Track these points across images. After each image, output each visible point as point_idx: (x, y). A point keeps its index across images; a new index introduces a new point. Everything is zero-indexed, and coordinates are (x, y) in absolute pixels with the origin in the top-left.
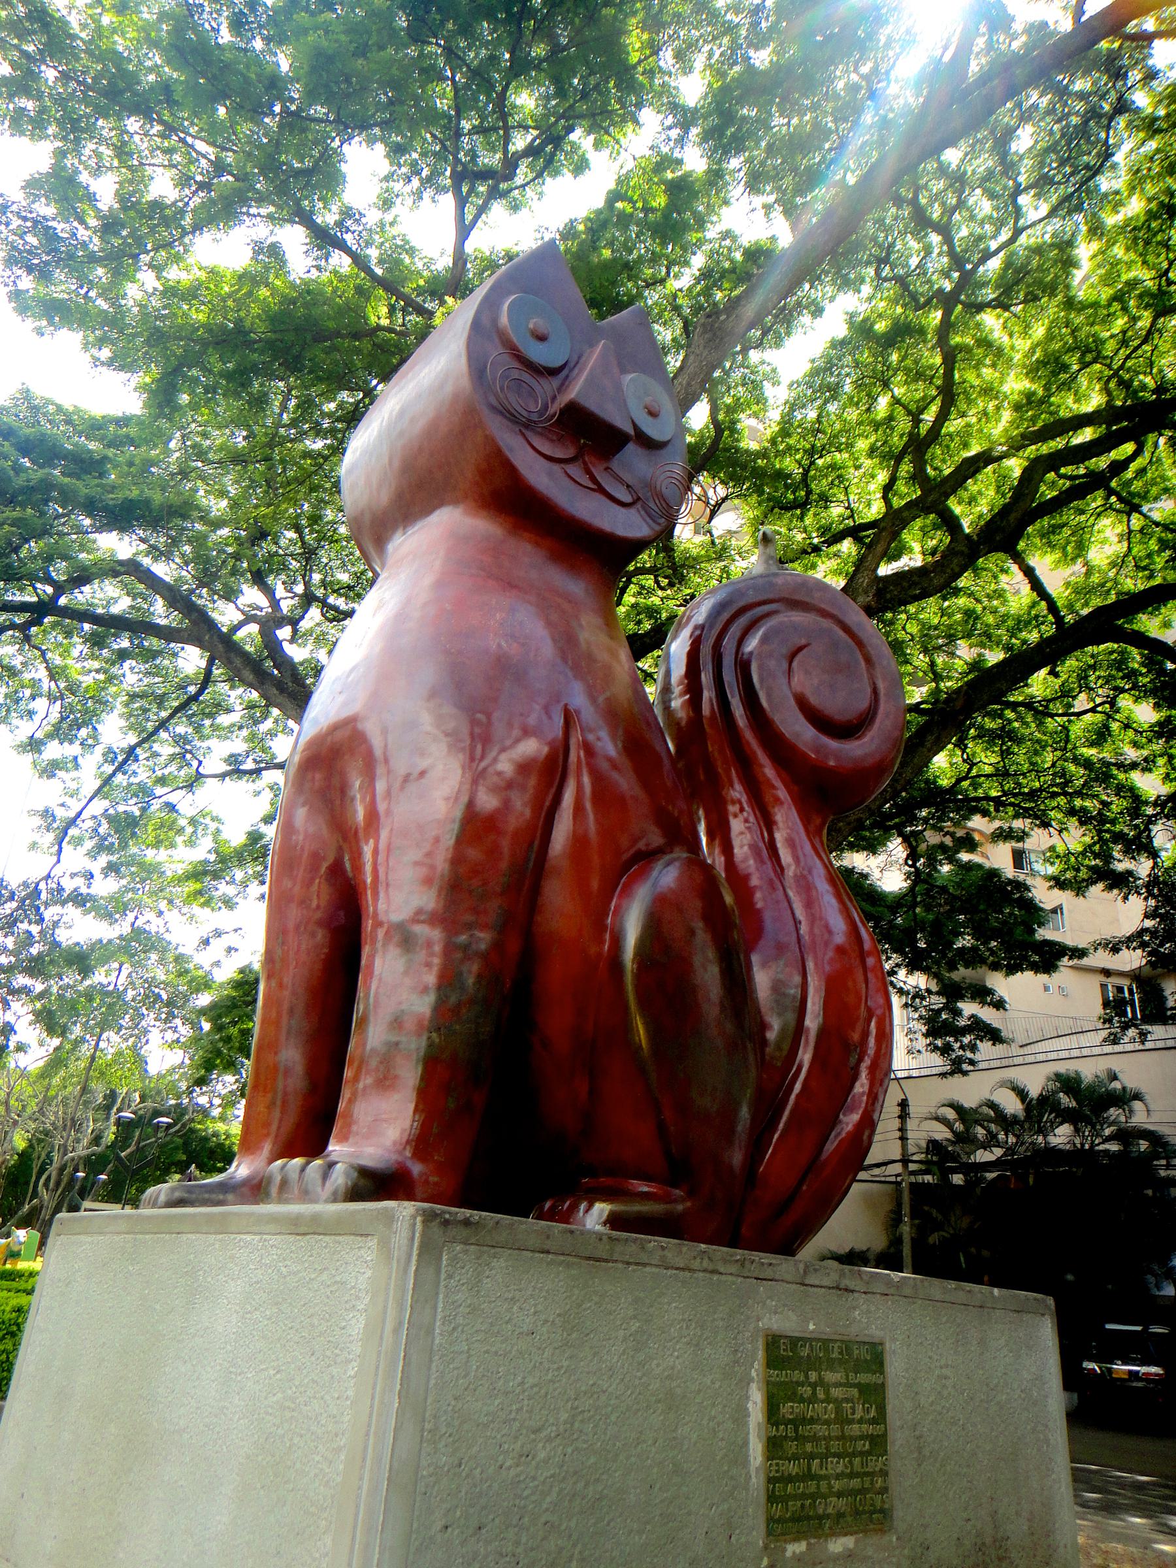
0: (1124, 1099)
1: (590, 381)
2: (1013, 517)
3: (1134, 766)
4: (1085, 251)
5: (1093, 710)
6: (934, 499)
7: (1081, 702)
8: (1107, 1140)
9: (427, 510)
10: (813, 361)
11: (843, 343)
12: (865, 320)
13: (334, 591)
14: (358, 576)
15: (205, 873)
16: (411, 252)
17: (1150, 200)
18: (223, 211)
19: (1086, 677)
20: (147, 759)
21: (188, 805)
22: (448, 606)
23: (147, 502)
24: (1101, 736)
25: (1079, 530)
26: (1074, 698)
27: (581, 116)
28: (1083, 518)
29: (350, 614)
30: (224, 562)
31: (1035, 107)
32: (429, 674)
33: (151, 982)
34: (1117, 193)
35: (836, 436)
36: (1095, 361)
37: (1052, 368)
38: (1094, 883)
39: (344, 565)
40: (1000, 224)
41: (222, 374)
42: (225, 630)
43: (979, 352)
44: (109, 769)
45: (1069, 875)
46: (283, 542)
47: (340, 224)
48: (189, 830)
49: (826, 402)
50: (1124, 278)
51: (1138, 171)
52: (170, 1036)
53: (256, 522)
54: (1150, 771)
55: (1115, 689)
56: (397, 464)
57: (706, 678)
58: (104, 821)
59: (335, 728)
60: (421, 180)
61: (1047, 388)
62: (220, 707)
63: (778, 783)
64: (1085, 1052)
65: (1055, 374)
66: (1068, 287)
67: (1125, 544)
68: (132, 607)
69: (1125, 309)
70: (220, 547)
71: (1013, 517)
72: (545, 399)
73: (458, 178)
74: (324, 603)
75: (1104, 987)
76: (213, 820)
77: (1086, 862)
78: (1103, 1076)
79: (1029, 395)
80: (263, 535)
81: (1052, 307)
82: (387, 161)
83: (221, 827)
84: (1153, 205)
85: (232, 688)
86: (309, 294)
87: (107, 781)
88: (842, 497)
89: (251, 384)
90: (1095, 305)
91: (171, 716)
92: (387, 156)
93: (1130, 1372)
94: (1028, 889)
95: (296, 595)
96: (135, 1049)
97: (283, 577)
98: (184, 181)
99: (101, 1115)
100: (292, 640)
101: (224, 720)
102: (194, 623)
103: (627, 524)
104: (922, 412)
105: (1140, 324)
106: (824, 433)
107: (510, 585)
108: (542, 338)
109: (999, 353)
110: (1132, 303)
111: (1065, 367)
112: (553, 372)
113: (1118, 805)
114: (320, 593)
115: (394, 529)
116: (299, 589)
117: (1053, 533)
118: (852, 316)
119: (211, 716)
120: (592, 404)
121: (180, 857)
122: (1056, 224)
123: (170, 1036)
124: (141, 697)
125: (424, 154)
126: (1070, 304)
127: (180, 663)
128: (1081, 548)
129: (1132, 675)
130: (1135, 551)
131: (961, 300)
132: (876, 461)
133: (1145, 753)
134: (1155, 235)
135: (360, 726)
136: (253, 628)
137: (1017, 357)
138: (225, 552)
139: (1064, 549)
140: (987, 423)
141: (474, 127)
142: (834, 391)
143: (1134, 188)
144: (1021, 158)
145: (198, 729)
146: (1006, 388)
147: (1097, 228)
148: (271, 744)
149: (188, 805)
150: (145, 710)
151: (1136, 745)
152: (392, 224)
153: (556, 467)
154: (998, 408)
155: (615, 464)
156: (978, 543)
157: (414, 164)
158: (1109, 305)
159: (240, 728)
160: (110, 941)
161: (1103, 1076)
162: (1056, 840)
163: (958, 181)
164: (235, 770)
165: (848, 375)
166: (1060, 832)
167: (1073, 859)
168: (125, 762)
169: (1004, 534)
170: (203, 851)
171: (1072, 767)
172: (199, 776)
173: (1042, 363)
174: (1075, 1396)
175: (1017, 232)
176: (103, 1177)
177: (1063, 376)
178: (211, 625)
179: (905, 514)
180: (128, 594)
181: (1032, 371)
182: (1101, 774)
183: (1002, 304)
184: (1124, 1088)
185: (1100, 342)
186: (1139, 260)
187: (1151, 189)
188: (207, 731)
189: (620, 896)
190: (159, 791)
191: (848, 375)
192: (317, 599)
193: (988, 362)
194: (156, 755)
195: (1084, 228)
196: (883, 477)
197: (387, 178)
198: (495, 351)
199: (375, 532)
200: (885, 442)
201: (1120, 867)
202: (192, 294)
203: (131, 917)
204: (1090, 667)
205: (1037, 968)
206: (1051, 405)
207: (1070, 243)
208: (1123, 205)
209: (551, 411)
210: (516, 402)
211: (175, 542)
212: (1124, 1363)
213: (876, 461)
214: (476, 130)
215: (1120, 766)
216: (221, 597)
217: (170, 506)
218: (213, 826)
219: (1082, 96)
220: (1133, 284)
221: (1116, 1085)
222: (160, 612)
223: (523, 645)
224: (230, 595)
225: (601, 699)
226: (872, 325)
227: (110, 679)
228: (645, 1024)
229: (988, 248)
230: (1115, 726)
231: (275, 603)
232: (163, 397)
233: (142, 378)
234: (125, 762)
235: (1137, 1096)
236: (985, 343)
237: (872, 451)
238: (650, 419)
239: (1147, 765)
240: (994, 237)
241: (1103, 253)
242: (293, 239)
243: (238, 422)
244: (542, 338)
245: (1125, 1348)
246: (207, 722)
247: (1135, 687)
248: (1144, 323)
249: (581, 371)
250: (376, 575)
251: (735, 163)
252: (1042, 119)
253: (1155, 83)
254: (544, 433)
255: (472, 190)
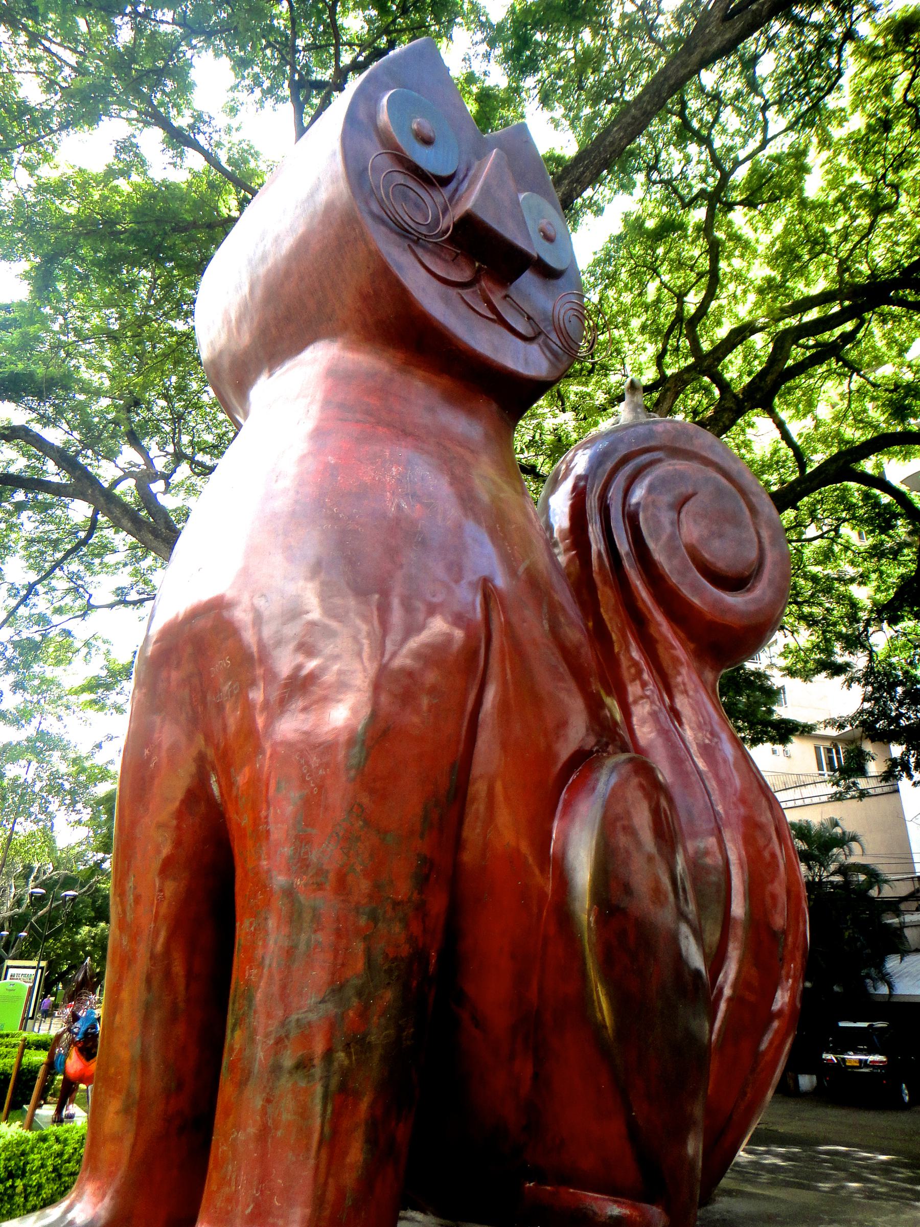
0: (843, 841)
1: (486, 191)
2: (769, 379)
3: (852, 580)
4: (815, 158)
5: (821, 537)
6: (708, 364)
7: (811, 531)
8: (833, 874)
9: (296, 346)
10: (595, 253)
11: (619, 238)
12: (638, 218)
13: (200, 450)
14: (220, 437)
15: (98, 686)
16: (256, 155)
17: (871, 116)
18: (86, 106)
19: (815, 510)
20: (46, 593)
21: (81, 630)
22: (331, 460)
23: (31, 375)
24: (827, 556)
25: (810, 390)
26: (806, 527)
27: (401, 31)
28: (812, 381)
29: (212, 469)
30: (105, 427)
31: (776, 36)
32: (311, 542)
33: (54, 776)
34: (842, 110)
35: (614, 316)
36: (823, 251)
37: (787, 258)
38: (819, 672)
39: (208, 427)
40: (748, 135)
41: (93, 263)
42: (106, 485)
43: (730, 244)
44: (13, 602)
45: (799, 666)
46: (156, 409)
47: (192, 127)
48: (84, 651)
49: (606, 287)
50: (848, 182)
51: (860, 92)
52: (74, 817)
53: (131, 392)
54: (865, 584)
55: (838, 519)
56: (259, 293)
57: (594, 532)
58: (9, 646)
59: (195, 614)
60: (263, 91)
61: (783, 275)
62: (106, 548)
63: (676, 643)
64: (808, 801)
65: (790, 263)
66: (801, 190)
67: (846, 402)
68: (28, 466)
69: (846, 209)
70: (102, 413)
71: (769, 379)
72: (435, 212)
73: (296, 87)
74: (192, 461)
75: (817, 749)
76: (104, 642)
77: (813, 656)
78: (827, 824)
79: (770, 280)
80: (137, 403)
81: (789, 208)
82: (232, 73)
83: (110, 648)
84: (873, 121)
85: (116, 532)
86: (168, 191)
87: (12, 613)
88: (618, 366)
89: (120, 271)
90: (823, 205)
91: (65, 558)
92: (233, 68)
93: (860, 1061)
94: (767, 677)
95: (168, 453)
96: (44, 831)
97: (157, 439)
98: (50, 86)
99: (21, 882)
100: (166, 492)
101: (110, 559)
102: (78, 479)
103: (526, 360)
104: (686, 295)
105: (858, 221)
106: (605, 314)
107: (404, 432)
108: (427, 141)
109: (746, 245)
110: (853, 204)
111: (798, 258)
112: (444, 181)
113: (839, 611)
114: (189, 451)
115: (258, 373)
116: (170, 448)
117: (789, 393)
118: (627, 215)
119: (100, 555)
120: (489, 218)
121: (76, 673)
122: (792, 136)
123: (74, 817)
124: (38, 542)
125: (265, 68)
126: (803, 204)
127: (70, 513)
128: (810, 405)
129: (851, 507)
130: (853, 406)
131: (717, 200)
132: (647, 336)
133: (861, 570)
134: (873, 146)
135: (225, 614)
136: (131, 483)
137: (761, 249)
138: (106, 418)
139: (797, 406)
140: (738, 306)
141: (307, 45)
142: (613, 278)
143: (857, 107)
144: (765, 80)
145: (89, 566)
146: (751, 275)
147: (825, 141)
148: (151, 577)
149: (81, 630)
150: (42, 553)
151: (852, 563)
152: (237, 129)
153: (453, 292)
154: (745, 292)
155: (512, 290)
156: (743, 401)
157: (256, 77)
158: (835, 205)
159: (125, 565)
160: (19, 743)
161: (827, 824)
162: (790, 640)
163: (715, 99)
164: (122, 599)
165: (623, 265)
166: (792, 633)
167: (802, 653)
168: (26, 597)
169: (763, 392)
170: (96, 668)
171: (802, 582)
172: (90, 607)
173: (780, 254)
174: (814, 1077)
175: (765, 143)
176: (24, 934)
177: (797, 265)
178: (93, 481)
179: (685, 377)
180: (23, 455)
181: (773, 260)
182: (825, 586)
183: (750, 203)
184: (844, 833)
185: (825, 236)
186: (859, 167)
187: (870, 107)
188: (97, 568)
189: (562, 818)
190: (56, 619)
191: (623, 265)
192: (185, 457)
193: (737, 253)
194: (54, 589)
195: (815, 140)
196: (652, 349)
197: (234, 88)
198: (374, 153)
199: (236, 378)
200: (654, 321)
201: (840, 660)
202: (60, 189)
203: (35, 722)
204: (818, 501)
205: (773, 740)
206: (787, 288)
207: (804, 153)
208: (847, 120)
209: (443, 225)
210: (404, 212)
211: (59, 411)
212: (855, 1054)
213: (647, 336)
214: (307, 48)
215: (840, 580)
216: (104, 457)
217: (52, 379)
218: (104, 648)
219: (817, 27)
220: (853, 187)
221: (838, 830)
222: (52, 472)
223: (428, 506)
224: (111, 455)
225: (521, 570)
226: (644, 222)
227: (11, 527)
228: (609, 995)
229: (736, 158)
230: (836, 548)
231: (149, 462)
232: (42, 281)
233: (24, 266)
234: (26, 597)
235: (854, 838)
236: (736, 238)
237: (643, 328)
238: (547, 243)
239: (863, 579)
240: (743, 147)
241: (830, 161)
242: (151, 140)
243: (110, 303)
244: (427, 141)
245: (853, 1041)
246: (97, 561)
247: (854, 517)
248: (864, 220)
249: (472, 183)
250: (239, 426)
251: (529, 82)
252: (783, 47)
253: (877, 15)
254: (437, 250)
255: (307, 99)
